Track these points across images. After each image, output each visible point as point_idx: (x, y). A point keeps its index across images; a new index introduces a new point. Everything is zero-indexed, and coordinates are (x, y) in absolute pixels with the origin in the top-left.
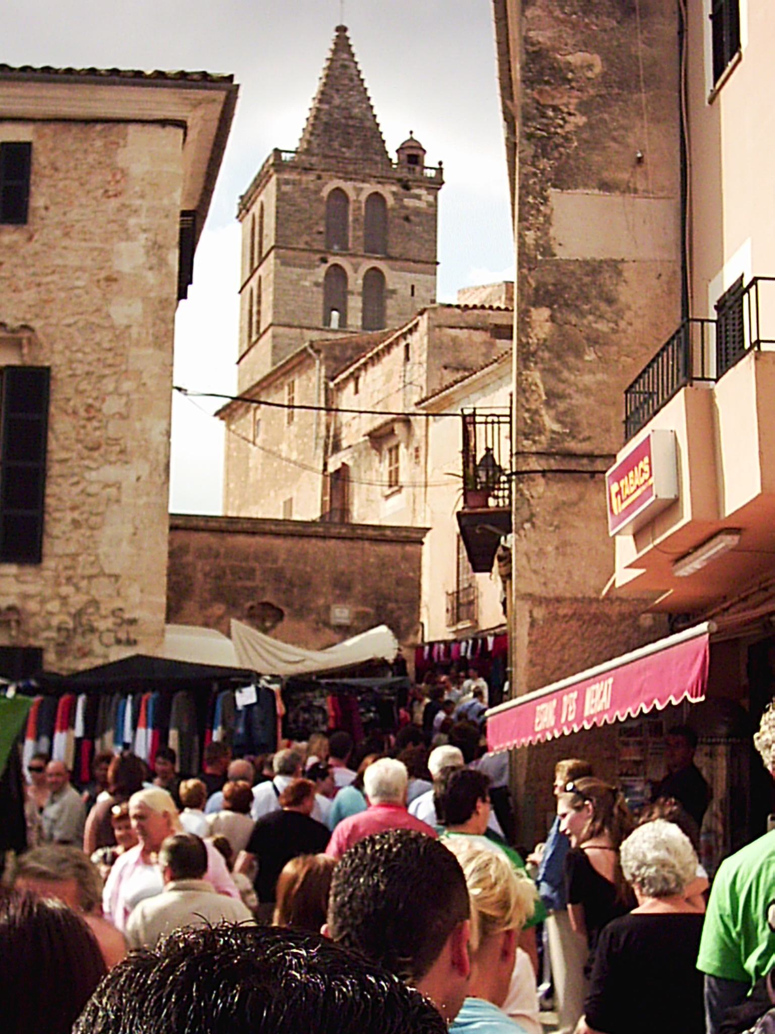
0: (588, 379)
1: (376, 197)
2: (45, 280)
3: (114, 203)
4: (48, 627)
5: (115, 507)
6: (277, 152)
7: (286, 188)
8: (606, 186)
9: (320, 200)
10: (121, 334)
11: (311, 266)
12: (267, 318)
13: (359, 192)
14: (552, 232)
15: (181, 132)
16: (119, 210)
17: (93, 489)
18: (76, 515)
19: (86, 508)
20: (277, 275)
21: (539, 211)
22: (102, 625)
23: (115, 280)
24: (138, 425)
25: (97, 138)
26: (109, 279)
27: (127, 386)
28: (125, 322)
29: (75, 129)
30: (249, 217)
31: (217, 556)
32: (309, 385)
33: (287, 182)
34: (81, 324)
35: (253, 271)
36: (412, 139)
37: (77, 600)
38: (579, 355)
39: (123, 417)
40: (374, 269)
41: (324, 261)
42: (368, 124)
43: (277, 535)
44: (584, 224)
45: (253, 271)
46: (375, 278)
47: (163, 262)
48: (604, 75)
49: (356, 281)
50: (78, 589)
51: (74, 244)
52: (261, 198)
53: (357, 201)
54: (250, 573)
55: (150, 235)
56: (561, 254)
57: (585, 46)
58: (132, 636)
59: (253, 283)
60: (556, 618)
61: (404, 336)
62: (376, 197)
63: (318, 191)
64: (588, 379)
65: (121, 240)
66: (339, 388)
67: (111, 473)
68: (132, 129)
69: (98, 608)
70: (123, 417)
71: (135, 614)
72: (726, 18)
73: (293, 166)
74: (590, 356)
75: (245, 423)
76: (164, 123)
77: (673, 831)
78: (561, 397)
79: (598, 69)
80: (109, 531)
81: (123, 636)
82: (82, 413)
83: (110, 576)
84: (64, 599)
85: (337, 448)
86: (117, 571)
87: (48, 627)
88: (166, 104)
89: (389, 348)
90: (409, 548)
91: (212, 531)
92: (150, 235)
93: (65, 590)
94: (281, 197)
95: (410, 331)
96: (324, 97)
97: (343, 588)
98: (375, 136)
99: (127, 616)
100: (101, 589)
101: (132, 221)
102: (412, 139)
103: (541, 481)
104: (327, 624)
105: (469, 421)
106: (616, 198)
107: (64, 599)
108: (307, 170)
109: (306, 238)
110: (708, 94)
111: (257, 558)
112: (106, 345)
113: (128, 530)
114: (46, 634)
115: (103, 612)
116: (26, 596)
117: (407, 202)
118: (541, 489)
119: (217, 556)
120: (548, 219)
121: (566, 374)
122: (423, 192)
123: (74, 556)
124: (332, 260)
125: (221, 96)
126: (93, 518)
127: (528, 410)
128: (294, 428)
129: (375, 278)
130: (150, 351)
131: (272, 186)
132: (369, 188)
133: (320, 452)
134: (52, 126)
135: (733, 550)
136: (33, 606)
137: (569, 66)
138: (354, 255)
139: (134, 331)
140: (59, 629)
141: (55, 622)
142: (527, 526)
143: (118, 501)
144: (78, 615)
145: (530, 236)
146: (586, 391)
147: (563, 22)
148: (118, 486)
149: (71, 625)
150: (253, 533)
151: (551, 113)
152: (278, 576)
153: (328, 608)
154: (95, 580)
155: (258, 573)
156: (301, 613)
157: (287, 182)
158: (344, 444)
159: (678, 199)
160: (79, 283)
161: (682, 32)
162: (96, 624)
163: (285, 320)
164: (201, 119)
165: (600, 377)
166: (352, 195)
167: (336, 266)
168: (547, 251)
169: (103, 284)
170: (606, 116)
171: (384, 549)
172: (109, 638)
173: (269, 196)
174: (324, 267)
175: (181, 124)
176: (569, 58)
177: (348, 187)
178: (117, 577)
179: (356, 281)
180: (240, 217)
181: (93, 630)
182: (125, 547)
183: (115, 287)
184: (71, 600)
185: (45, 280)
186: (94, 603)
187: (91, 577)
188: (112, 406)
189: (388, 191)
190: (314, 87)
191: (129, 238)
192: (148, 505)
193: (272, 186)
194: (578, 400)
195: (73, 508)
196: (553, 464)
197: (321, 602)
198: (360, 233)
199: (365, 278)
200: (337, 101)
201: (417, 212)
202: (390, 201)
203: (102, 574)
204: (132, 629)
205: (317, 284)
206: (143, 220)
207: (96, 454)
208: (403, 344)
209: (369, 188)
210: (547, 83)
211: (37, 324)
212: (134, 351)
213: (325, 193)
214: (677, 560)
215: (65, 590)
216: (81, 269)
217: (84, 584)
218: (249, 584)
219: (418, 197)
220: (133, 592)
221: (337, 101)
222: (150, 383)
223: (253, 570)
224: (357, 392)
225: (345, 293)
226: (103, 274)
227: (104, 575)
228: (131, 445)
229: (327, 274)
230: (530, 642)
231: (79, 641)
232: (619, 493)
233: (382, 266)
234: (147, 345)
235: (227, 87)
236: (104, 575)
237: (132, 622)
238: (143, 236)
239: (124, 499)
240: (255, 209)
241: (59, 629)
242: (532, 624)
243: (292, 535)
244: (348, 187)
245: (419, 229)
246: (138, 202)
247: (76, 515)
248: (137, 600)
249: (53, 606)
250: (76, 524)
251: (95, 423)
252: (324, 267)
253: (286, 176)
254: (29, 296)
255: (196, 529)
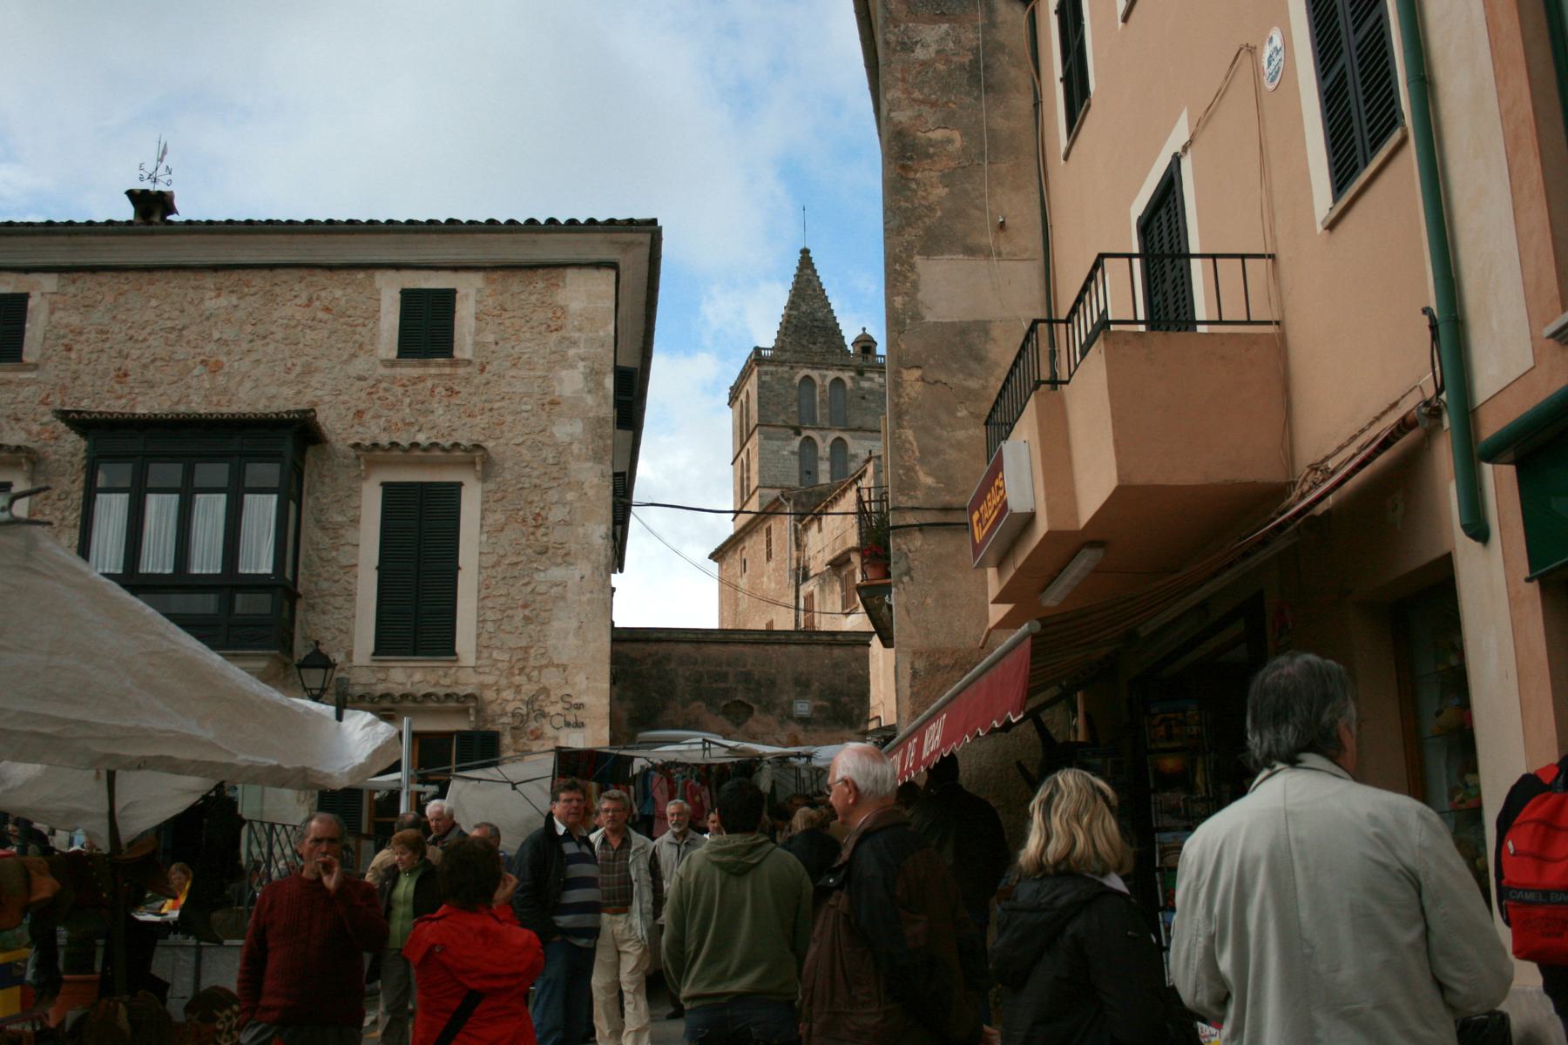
0: (961, 434)
1: (838, 380)
2: (496, 405)
3: (555, 336)
4: (504, 714)
5: (562, 604)
6: (757, 350)
7: (767, 378)
8: (971, 251)
9: (793, 386)
10: (562, 450)
11: (788, 439)
12: (755, 482)
13: (824, 378)
14: (920, 296)
15: (612, 274)
16: (560, 342)
17: (542, 588)
18: (527, 612)
19: (537, 605)
20: (761, 448)
21: (906, 277)
22: (552, 710)
23: (558, 403)
24: (581, 530)
25: (539, 282)
26: (552, 403)
27: (570, 496)
28: (568, 440)
29: (520, 275)
30: (738, 404)
31: (695, 663)
32: (783, 527)
33: (766, 373)
34: (529, 443)
35: (743, 446)
36: (864, 334)
37: (529, 689)
38: (952, 412)
39: (566, 523)
40: (839, 439)
41: (798, 433)
42: (830, 324)
43: (745, 643)
44: (950, 289)
45: (743, 446)
46: (839, 444)
47: (600, 385)
48: (964, 149)
49: (824, 449)
50: (530, 680)
51: (522, 373)
52: (747, 387)
53: (823, 385)
54: (724, 677)
55: (588, 363)
56: (930, 318)
57: (944, 124)
58: (580, 720)
59: (743, 455)
60: (938, 668)
61: (855, 481)
62: (838, 380)
63: (791, 379)
64: (961, 434)
65: (564, 368)
66: (806, 528)
67: (557, 573)
68: (571, 274)
69: (548, 696)
70: (566, 523)
71: (584, 699)
72: (1075, 78)
73: (770, 361)
74: (962, 413)
75: (734, 560)
76: (598, 265)
77: (805, 809)
78: (937, 453)
79: (958, 144)
80: (556, 624)
81: (572, 719)
82: (531, 522)
83: (558, 666)
84: (518, 688)
85: (806, 578)
86: (564, 660)
87: (504, 714)
88: (600, 249)
89: (845, 491)
90: (859, 650)
91: (691, 641)
92: (588, 363)
93: (517, 679)
94: (762, 386)
95: (860, 477)
96: (792, 305)
97: (803, 685)
98: (834, 332)
99: (574, 701)
100: (551, 678)
101: (572, 352)
102: (864, 334)
103: (918, 535)
104: (790, 717)
105: (858, 490)
106: (980, 263)
107: (518, 688)
108: (782, 363)
109: (783, 417)
110: (1063, 150)
111: (729, 665)
112: (551, 461)
113: (574, 624)
114: (505, 720)
115: (553, 698)
116: (483, 686)
117: (866, 384)
118: (918, 543)
119: (695, 663)
120: (915, 286)
121: (938, 431)
122: (876, 376)
123: (526, 649)
124: (805, 433)
125: (646, 238)
126: (543, 614)
127: (902, 467)
128: (772, 564)
129: (839, 444)
130: (590, 464)
131: (754, 377)
132: (832, 374)
133: (793, 582)
134: (500, 273)
135: (1095, 571)
136: (489, 695)
137: (930, 143)
138: (822, 429)
139: (575, 448)
140: (514, 715)
141: (510, 708)
142: (906, 579)
143: (563, 598)
144: (530, 702)
145: (899, 301)
146: (959, 446)
147: (922, 102)
148: (563, 584)
149: (524, 711)
150: (726, 643)
151: (914, 186)
152: (747, 677)
153: (791, 703)
154: (545, 671)
155: (731, 677)
156: (768, 708)
157: (766, 373)
158: (812, 573)
159: (1040, 262)
160: (524, 407)
161: (1037, 104)
162: (547, 710)
163: (769, 483)
164: (632, 264)
165: (971, 432)
166: (818, 381)
167: (808, 438)
168: (917, 317)
169: (547, 408)
170: (968, 186)
171: (837, 652)
172: (559, 721)
173: (752, 386)
174: (799, 439)
175: (613, 266)
176: (930, 134)
177: (815, 374)
178: (565, 668)
179: (824, 449)
180: (731, 403)
181: (544, 715)
182: (572, 640)
183: (557, 409)
184: (524, 689)
185: (496, 405)
186: (545, 691)
187: (540, 668)
188: (556, 514)
189: (847, 376)
190: (784, 299)
191: (573, 367)
192: (590, 602)
193: (754, 377)
194: (952, 454)
195: (525, 606)
196: (930, 518)
197: (785, 698)
198: (826, 411)
199: (832, 446)
200: (804, 308)
201: (871, 391)
202: (849, 384)
203: (551, 664)
204: (579, 713)
205: (793, 453)
206: (582, 350)
207: (544, 558)
208: (854, 488)
209: (832, 374)
210: (911, 158)
211: (490, 444)
212: (574, 466)
213: (797, 380)
214: (1043, 590)
215: (517, 679)
216: (529, 395)
217: (535, 673)
218: (723, 685)
219: (871, 380)
220: (580, 680)
221: (804, 308)
222: (591, 493)
223: (726, 674)
224: (820, 530)
225: (816, 459)
226: (548, 398)
227: (553, 665)
228: (573, 547)
229: (802, 444)
230: (912, 694)
231: (533, 725)
232: (980, 520)
233: (846, 436)
234: (587, 460)
235: (651, 228)
236: (553, 665)
237: (580, 706)
238: (581, 365)
239: (569, 595)
240: (743, 397)
241: (514, 715)
242: (915, 675)
243: (756, 642)
244: (815, 374)
245: (873, 405)
246: (577, 335)
247: (527, 612)
248: (584, 686)
249: (508, 694)
250: (526, 618)
251: (542, 530)
252: (799, 439)
253: (765, 368)
254: (481, 421)
255: (678, 641)
